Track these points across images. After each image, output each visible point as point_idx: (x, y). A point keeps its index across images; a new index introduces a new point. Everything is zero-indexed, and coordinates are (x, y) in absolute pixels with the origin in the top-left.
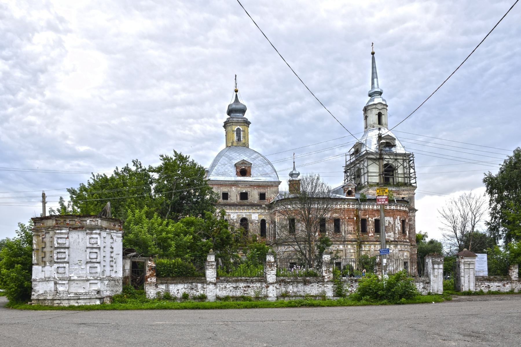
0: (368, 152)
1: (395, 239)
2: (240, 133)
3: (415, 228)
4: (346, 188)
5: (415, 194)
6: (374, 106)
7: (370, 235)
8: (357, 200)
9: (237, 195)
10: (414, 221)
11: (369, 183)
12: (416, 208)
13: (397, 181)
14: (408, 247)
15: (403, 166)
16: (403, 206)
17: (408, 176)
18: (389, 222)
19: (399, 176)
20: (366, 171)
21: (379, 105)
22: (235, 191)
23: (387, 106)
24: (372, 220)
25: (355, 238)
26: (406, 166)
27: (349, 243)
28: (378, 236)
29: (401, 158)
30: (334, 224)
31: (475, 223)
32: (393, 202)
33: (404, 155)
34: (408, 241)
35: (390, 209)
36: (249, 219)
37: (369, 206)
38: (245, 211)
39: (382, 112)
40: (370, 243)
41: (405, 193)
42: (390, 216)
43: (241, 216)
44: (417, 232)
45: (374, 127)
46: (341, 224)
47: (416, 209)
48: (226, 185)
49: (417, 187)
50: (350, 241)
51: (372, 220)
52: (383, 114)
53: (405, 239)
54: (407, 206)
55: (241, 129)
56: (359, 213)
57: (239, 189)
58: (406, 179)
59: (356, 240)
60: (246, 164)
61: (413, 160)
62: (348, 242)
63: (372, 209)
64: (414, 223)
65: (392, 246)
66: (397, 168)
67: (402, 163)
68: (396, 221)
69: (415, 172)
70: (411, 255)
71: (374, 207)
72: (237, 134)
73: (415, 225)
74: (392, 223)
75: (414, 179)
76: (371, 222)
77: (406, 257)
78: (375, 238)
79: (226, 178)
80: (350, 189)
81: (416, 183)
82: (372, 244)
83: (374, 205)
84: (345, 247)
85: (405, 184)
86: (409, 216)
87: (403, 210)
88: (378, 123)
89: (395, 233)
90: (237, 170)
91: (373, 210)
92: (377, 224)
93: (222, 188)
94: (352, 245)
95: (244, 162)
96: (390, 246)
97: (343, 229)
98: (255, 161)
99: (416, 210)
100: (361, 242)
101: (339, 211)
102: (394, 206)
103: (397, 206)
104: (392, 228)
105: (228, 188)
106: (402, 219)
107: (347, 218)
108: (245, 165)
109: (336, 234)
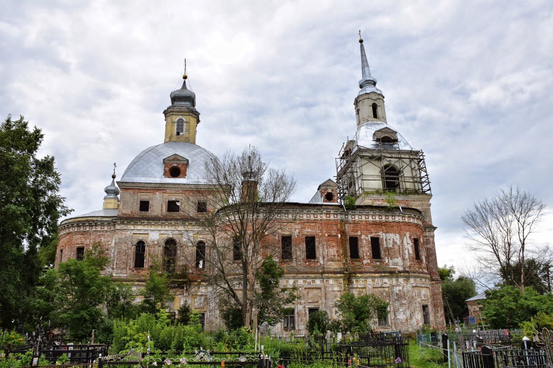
0: (360, 149)
1: (404, 268)
2: (182, 125)
3: (435, 254)
4: (324, 190)
5: (430, 205)
6: (367, 96)
7: (365, 262)
8: (341, 206)
9: (162, 205)
10: (434, 243)
11: (366, 190)
12: (434, 225)
13: (404, 187)
14: (427, 280)
15: (411, 167)
16: (413, 218)
17: (419, 180)
18: (393, 241)
19: (406, 180)
20: (359, 174)
21: (372, 94)
22: (159, 198)
23: (384, 97)
24: (367, 238)
25: (340, 268)
26: (415, 167)
27: (331, 275)
28: (378, 263)
29: (407, 156)
30: (305, 246)
31: (511, 254)
32: (397, 211)
33: (411, 152)
34: (426, 271)
35: (394, 222)
36: (178, 240)
37: (360, 217)
38: (173, 228)
39: (377, 103)
40: (365, 275)
41: (417, 204)
42: (395, 232)
43: (166, 236)
44: (440, 265)
45: (368, 121)
46: (317, 244)
47: (435, 226)
48: (147, 190)
49: (432, 196)
50: (331, 273)
51: (367, 238)
52: (378, 105)
53: (421, 268)
54: (419, 217)
55: (185, 120)
56: (345, 229)
57: (166, 195)
58: (416, 184)
59: (343, 270)
60: (179, 160)
61: (423, 159)
62: (328, 273)
63: (366, 221)
64: (434, 247)
65: (401, 280)
66: (402, 169)
67: (408, 163)
68: (405, 239)
69: (427, 175)
70: (434, 295)
71: (368, 218)
72: (178, 125)
73: (435, 250)
74: (398, 242)
75: (427, 185)
76: (364, 241)
77: (425, 297)
78: (374, 267)
79: (148, 180)
80: (330, 191)
81: (430, 190)
82: (369, 277)
83: (368, 215)
84: (323, 282)
85: (416, 192)
86: (426, 236)
87: (414, 224)
88: (373, 116)
89: (404, 259)
90: (166, 169)
91: (367, 223)
92: (375, 243)
93: (140, 194)
94: (336, 279)
95: (176, 157)
96: (397, 280)
97: (321, 253)
98: (195, 157)
99: (435, 228)
100: (350, 274)
101: (314, 224)
102: (399, 216)
103: (404, 217)
104: (400, 251)
105: (149, 194)
106: (413, 237)
107: (326, 235)
108: (178, 162)
109: (309, 261)
